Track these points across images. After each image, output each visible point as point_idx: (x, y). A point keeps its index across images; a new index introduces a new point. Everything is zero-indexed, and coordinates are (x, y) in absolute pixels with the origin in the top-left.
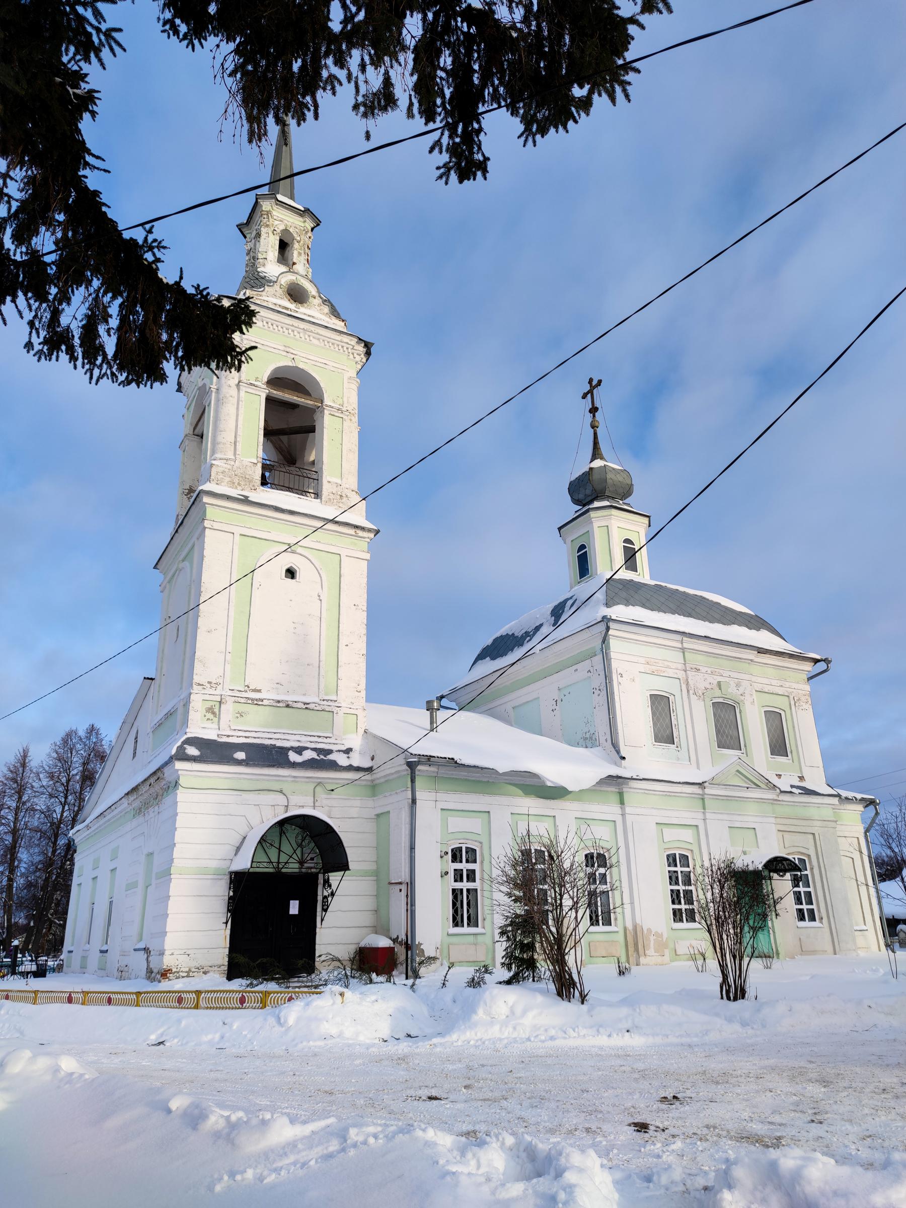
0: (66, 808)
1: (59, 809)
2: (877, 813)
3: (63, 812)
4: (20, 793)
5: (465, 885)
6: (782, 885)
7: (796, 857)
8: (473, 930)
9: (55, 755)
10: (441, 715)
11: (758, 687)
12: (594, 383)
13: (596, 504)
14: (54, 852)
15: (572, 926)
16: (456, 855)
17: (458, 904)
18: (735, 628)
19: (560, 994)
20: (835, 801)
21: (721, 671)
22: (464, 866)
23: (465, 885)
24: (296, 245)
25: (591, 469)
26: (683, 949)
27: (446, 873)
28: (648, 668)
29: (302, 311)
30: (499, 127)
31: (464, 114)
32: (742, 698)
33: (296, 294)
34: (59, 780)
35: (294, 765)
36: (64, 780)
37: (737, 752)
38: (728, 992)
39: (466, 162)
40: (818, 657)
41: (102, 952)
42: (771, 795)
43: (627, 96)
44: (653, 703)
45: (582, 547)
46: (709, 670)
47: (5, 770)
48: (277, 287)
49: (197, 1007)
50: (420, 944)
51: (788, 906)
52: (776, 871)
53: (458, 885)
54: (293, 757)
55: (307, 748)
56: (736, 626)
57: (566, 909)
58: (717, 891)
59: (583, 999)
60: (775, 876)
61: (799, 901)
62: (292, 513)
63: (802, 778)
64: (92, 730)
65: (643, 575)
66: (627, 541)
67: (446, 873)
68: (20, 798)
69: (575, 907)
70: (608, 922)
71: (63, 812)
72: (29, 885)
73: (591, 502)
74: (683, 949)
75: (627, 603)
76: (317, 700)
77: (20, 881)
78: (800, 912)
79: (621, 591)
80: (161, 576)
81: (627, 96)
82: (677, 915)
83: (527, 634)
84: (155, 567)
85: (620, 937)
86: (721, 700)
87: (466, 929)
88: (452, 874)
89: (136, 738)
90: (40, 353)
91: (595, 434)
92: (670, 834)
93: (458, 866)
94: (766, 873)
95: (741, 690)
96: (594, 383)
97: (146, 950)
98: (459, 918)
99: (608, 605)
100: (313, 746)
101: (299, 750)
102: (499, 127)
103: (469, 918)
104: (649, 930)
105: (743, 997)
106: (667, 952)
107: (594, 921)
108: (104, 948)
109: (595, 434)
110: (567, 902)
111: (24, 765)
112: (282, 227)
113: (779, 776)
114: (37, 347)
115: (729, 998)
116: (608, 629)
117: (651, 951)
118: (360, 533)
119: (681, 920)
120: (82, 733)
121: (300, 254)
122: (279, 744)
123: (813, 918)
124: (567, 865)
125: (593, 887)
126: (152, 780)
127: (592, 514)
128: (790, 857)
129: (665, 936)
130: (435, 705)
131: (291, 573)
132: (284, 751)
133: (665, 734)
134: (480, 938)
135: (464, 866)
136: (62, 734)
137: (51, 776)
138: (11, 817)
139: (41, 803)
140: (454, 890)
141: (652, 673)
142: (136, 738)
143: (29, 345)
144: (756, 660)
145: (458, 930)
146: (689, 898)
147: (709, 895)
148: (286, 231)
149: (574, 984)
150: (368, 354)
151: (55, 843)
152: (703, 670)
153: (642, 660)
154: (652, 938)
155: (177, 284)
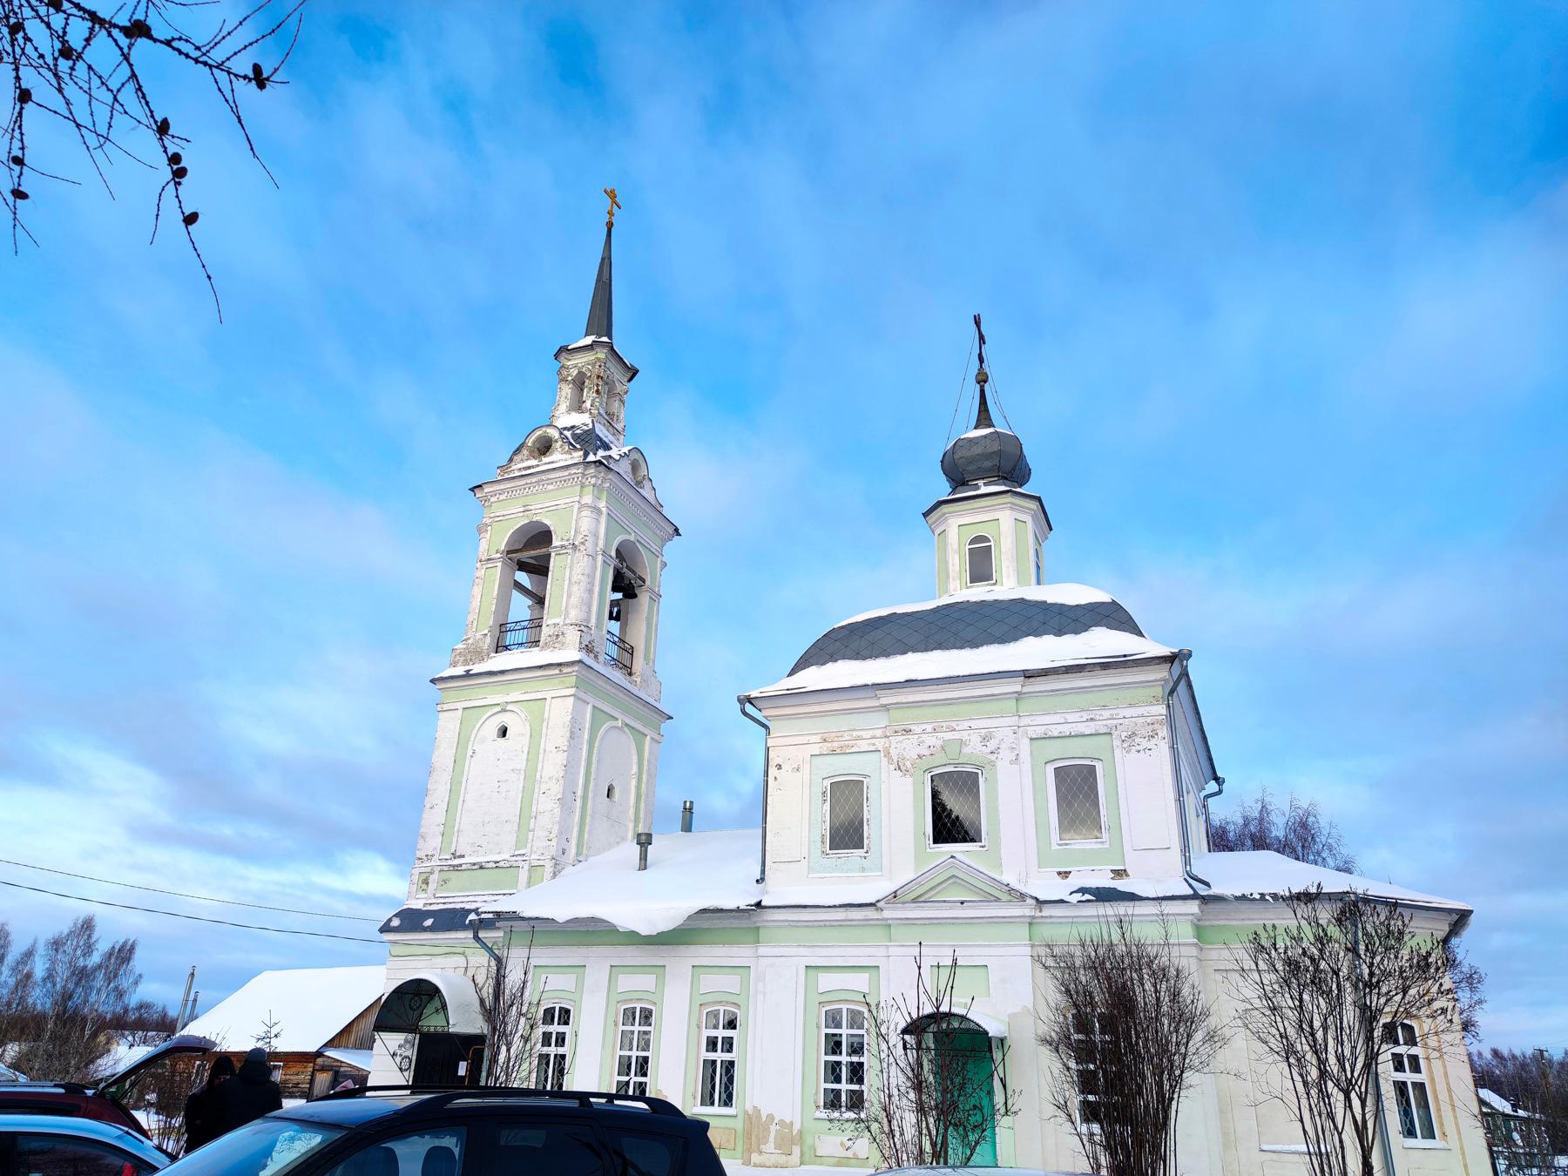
5: (720, 1056)
7: (844, 1007)
16: (630, 1015)
17: (725, 1079)
18: (1030, 642)
21: (953, 724)
22: (555, 1028)
23: (720, 1056)
28: (826, 747)
32: (993, 757)
46: (929, 728)
56: (1031, 638)
62: (503, 672)
70: (1430, 1134)
76: (507, 856)
82: (833, 1101)
85: (738, 1124)
86: (950, 769)
91: (982, 392)
92: (827, 981)
95: (992, 745)
104: (771, 1117)
106: (796, 1150)
109: (982, 392)
117: (770, 1146)
118: (565, 670)
131: (504, 732)
141: (833, 753)
144: (1026, 690)
146: (857, 1072)
152: (917, 729)
153: (817, 738)
154: (773, 1128)
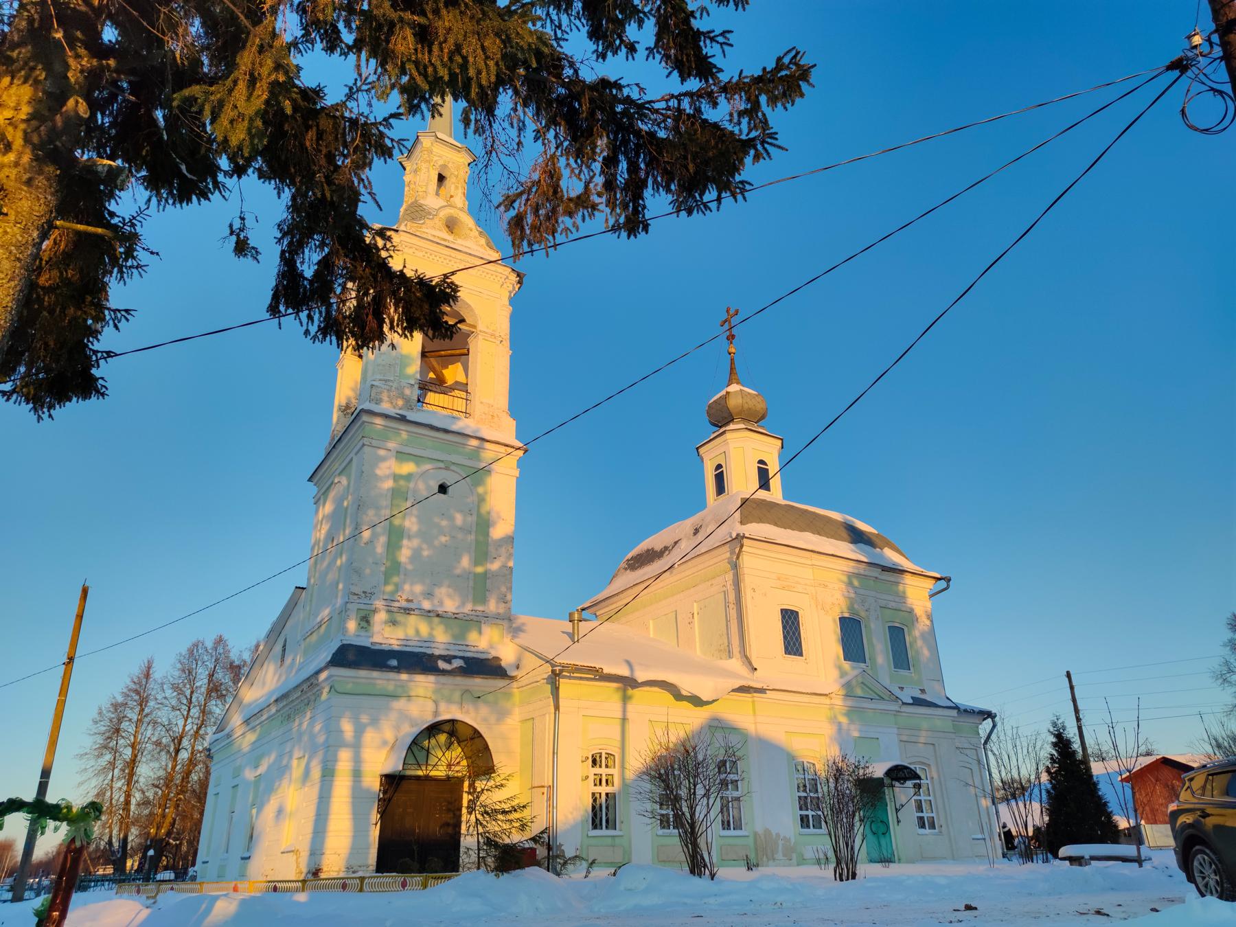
0: (190, 720)
1: (181, 722)
2: (994, 726)
3: (185, 726)
4: (143, 703)
6: (903, 793)
8: (611, 832)
9: (179, 666)
10: (584, 627)
11: (883, 603)
12: (732, 312)
13: (732, 426)
14: (173, 768)
15: (704, 812)
19: (692, 872)
20: (954, 713)
24: (453, 179)
25: (728, 393)
26: (809, 854)
27: (587, 777)
29: (459, 243)
30: (657, 202)
31: (635, 189)
33: (451, 225)
34: (182, 693)
35: (444, 672)
36: (188, 693)
37: (863, 665)
38: (841, 875)
39: (635, 224)
40: (938, 576)
41: (243, 859)
42: (894, 707)
43: (745, 198)
44: (783, 617)
45: (719, 466)
47: (128, 681)
48: (436, 220)
49: (361, 890)
50: (561, 845)
51: (910, 815)
52: (898, 779)
53: (598, 789)
54: (442, 665)
55: (455, 657)
57: (698, 797)
58: (832, 785)
59: (712, 876)
60: (897, 784)
61: (919, 808)
63: (923, 691)
64: (220, 641)
65: (776, 494)
66: (761, 462)
67: (587, 777)
68: (143, 710)
69: (707, 795)
71: (185, 726)
72: (145, 803)
73: (727, 424)
74: (809, 854)
75: (760, 521)
77: (137, 797)
78: (921, 819)
79: (751, 509)
80: (315, 489)
81: (745, 198)
82: (804, 821)
83: (666, 548)
84: (310, 480)
85: (751, 841)
87: (604, 832)
88: (592, 778)
89: (284, 646)
90: (315, 338)
93: (597, 770)
94: (887, 781)
96: (732, 312)
97: (555, 678)
98: (598, 821)
99: (742, 523)
100: (461, 654)
101: (448, 659)
102: (657, 202)
103: (607, 821)
105: (854, 877)
106: (794, 856)
107: (726, 825)
108: (246, 855)
110: (700, 791)
111: (147, 676)
112: (441, 162)
113: (902, 689)
114: (313, 333)
115: (841, 880)
116: (742, 546)
119: (808, 827)
120: (209, 644)
121: (457, 188)
122: (429, 651)
123: (933, 826)
124: (700, 758)
125: (723, 776)
126: (305, 687)
127: (728, 436)
128: (912, 767)
129: (793, 841)
130: (576, 617)
132: (433, 658)
133: (793, 644)
134: (617, 841)
135: (603, 771)
136: (188, 644)
137: (175, 687)
138: (132, 729)
139: (163, 715)
140: (593, 794)
142: (284, 646)
143: (307, 332)
144: (883, 577)
145: (597, 832)
147: (825, 789)
148: (444, 166)
149: (705, 866)
150: (520, 282)
151: (175, 760)
154: (781, 843)
155: (401, 271)
